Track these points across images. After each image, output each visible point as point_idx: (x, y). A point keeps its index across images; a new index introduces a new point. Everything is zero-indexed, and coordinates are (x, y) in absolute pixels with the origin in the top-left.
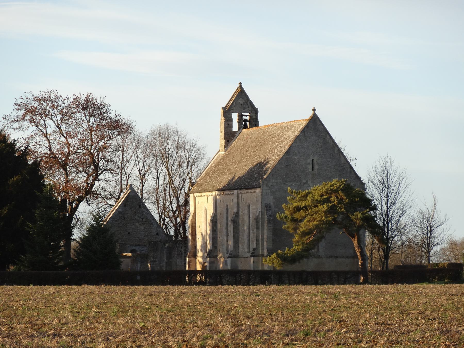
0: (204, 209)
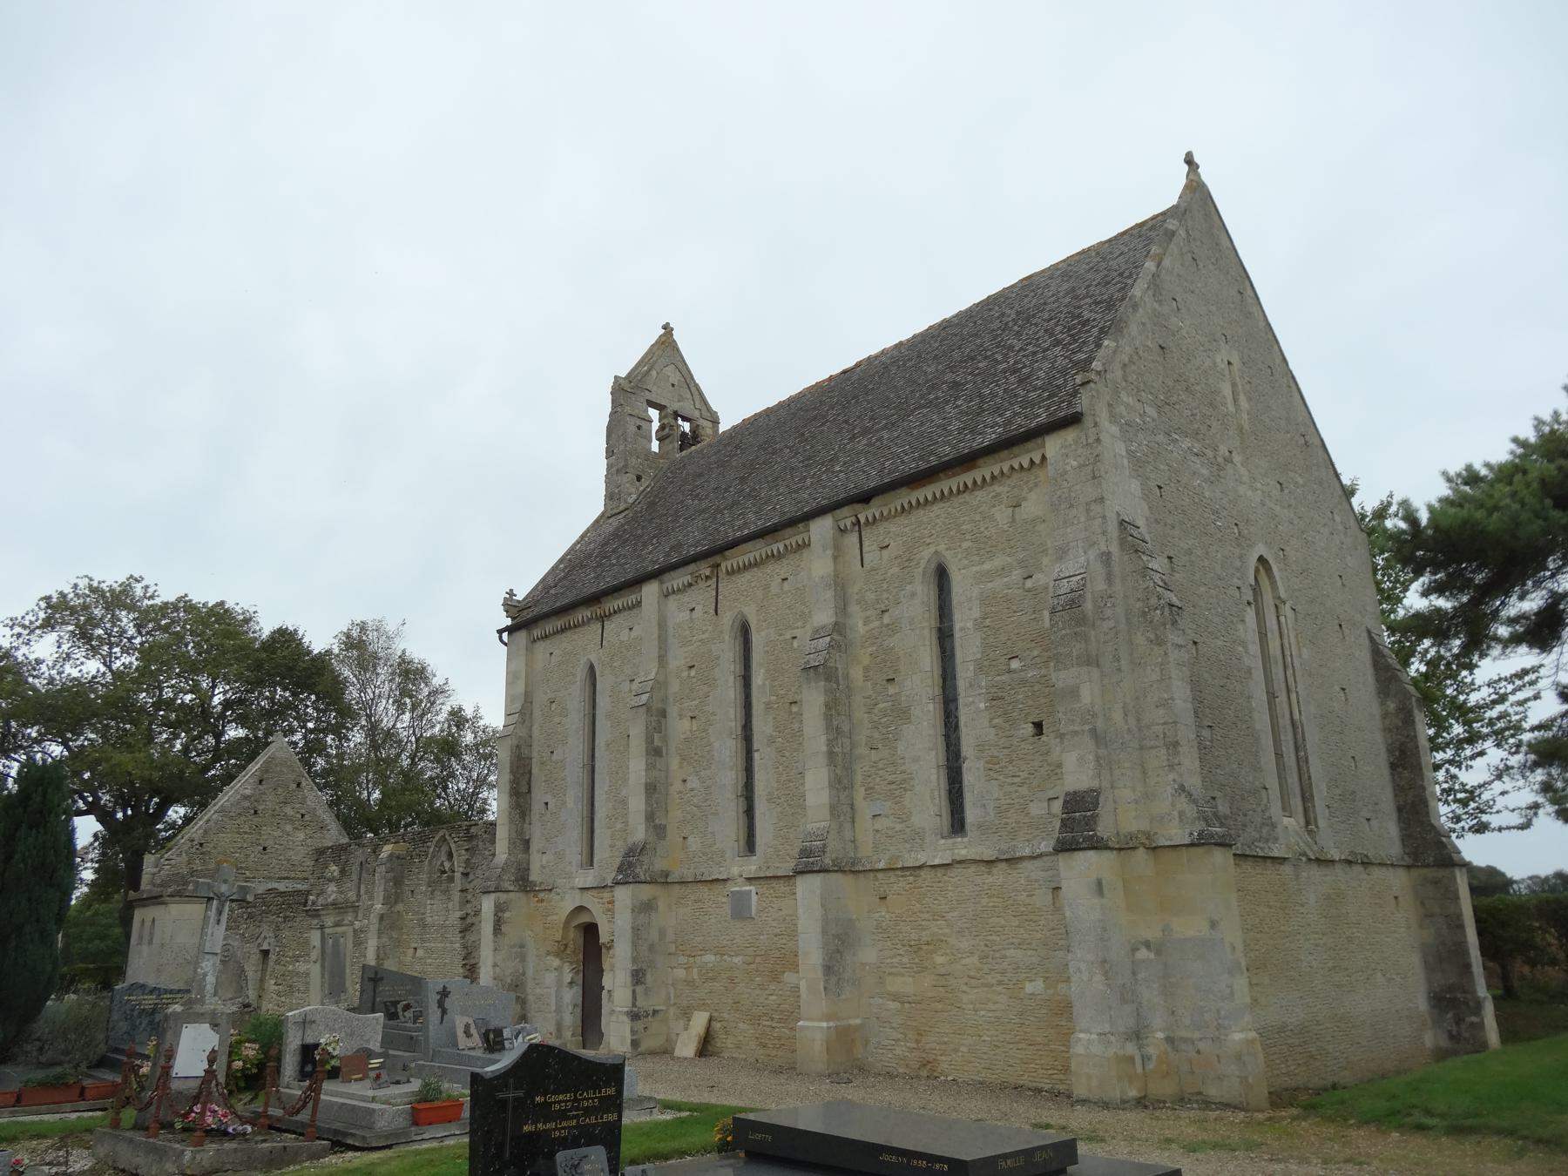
0: (581, 674)
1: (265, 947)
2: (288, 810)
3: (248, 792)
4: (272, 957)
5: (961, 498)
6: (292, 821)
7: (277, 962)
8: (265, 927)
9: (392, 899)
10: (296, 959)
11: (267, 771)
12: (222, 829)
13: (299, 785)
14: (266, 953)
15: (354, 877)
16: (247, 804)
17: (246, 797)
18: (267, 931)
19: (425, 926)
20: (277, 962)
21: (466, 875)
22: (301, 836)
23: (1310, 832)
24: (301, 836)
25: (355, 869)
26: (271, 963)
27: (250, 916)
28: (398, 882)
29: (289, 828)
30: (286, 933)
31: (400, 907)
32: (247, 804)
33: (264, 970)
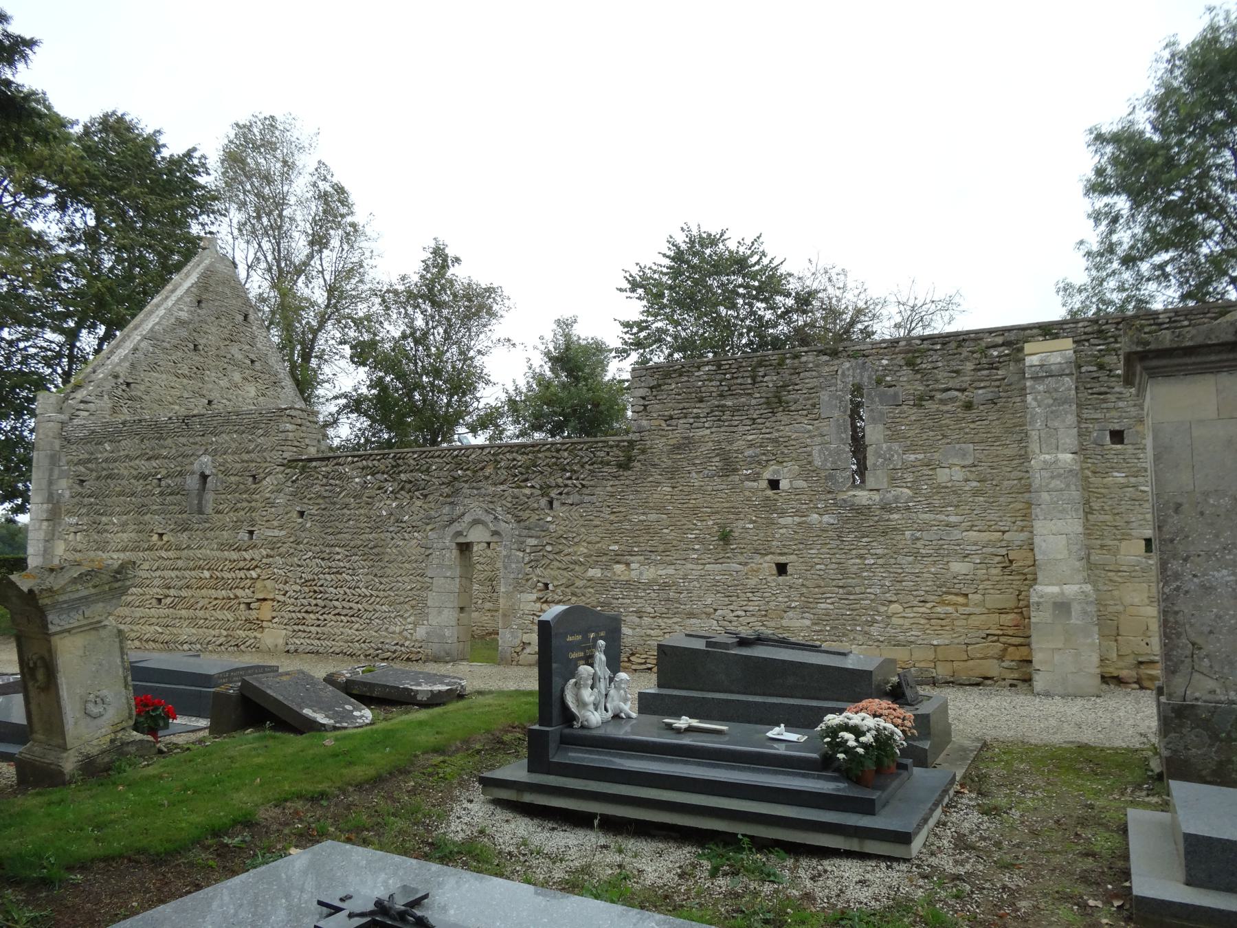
2: (234, 350)
3: (184, 315)
13: (246, 317)
16: (184, 333)
17: (182, 323)
32: (184, 333)
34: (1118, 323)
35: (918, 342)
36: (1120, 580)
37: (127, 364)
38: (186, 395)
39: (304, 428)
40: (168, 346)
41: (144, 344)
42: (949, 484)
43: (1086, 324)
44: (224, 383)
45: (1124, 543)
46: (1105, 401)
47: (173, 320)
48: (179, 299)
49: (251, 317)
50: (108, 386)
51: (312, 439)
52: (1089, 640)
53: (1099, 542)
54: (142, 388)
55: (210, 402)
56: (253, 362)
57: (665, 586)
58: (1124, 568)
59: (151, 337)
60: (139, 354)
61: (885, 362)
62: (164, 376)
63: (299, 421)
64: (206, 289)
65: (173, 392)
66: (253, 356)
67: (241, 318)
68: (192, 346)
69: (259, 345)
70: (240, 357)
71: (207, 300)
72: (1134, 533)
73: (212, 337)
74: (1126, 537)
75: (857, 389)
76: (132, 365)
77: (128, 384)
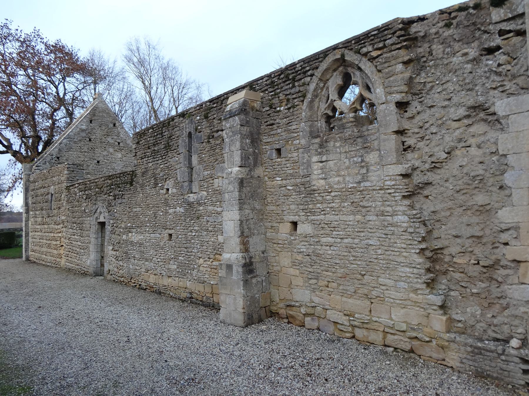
1: (102, 220)
2: (109, 139)
3: (84, 127)
4: (108, 228)
5: (374, 69)
6: (113, 146)
7: (113, 232)
8: (100, 204)
9: (251, 160)
10: (129, 230)
11: (94, 115)
12: (70, 149)
13: (114, 125)
14: (102, 225)
15: (182, 150)
16: (84, 134)
17: (83, 130)
18: (101, 207)
19: (311, 192)
20: (113, 232)
21: (402, 106)
22: (120, 155)
23: (447, 209)
24: (120, 155)
25: (182, 142)
26: (107, 233)
27: (88, 197)
28: (254, 139)
29: (111, 150)
30: (117, 209)
31: (259, 171)
32: (84, 134)
33: (103, 237)
34: (280, 75)
35: (208, 104)
36: (279, 250)
37: (57, 150)
38: (86, 160)
39: (75, 172)
40: (77, 140)
41: (65, 141)
42: (218, 189)
43: (266, 78)
44: (105, 153)
45: (281, 224)
46: (272, 130)
47: (78, 130)
48: (82, 120)
49: (117, 124)
50: (48, 159)
51: (79, 177)
52: (239, 291)
53: (270, 224)
54: (65, 158)
55: (98, 162)
56: (119, 143)
57: (141, 244)
58: (280, 242)
59: (68, 137)
60: (62, 145)
61: (198, 118)
62: (75, 153)
63: (72, 169)
64: (94, 115)
65: (79, 159)
66: (119, 141)
67: (112, 125)
68: (88, 139)
69: (121, 136)
70: (112, 141)
71: (95, 120)
72: (285, 218)
73: (98, 133)
74: (282, 221)
75: (190, 134)
76: (59, 149)
77: (58, 158)
